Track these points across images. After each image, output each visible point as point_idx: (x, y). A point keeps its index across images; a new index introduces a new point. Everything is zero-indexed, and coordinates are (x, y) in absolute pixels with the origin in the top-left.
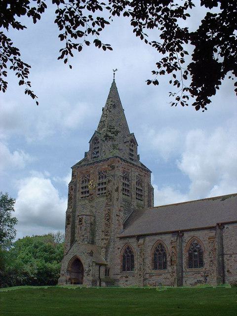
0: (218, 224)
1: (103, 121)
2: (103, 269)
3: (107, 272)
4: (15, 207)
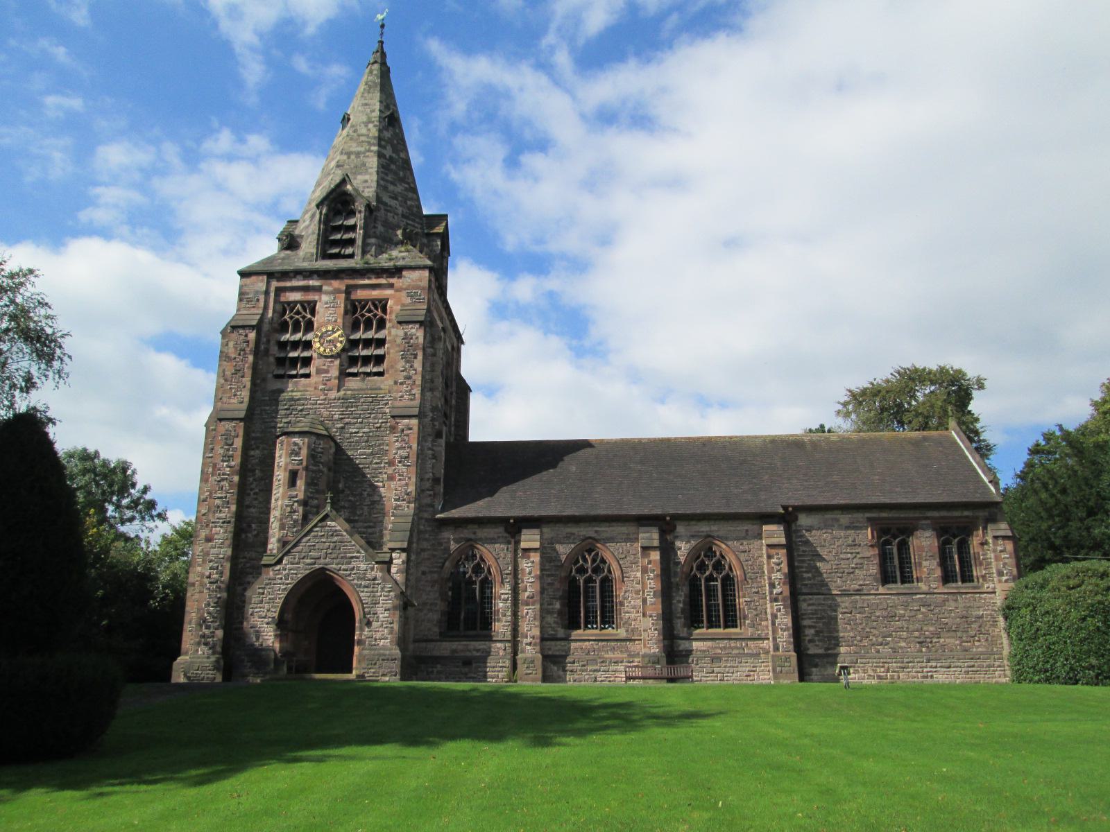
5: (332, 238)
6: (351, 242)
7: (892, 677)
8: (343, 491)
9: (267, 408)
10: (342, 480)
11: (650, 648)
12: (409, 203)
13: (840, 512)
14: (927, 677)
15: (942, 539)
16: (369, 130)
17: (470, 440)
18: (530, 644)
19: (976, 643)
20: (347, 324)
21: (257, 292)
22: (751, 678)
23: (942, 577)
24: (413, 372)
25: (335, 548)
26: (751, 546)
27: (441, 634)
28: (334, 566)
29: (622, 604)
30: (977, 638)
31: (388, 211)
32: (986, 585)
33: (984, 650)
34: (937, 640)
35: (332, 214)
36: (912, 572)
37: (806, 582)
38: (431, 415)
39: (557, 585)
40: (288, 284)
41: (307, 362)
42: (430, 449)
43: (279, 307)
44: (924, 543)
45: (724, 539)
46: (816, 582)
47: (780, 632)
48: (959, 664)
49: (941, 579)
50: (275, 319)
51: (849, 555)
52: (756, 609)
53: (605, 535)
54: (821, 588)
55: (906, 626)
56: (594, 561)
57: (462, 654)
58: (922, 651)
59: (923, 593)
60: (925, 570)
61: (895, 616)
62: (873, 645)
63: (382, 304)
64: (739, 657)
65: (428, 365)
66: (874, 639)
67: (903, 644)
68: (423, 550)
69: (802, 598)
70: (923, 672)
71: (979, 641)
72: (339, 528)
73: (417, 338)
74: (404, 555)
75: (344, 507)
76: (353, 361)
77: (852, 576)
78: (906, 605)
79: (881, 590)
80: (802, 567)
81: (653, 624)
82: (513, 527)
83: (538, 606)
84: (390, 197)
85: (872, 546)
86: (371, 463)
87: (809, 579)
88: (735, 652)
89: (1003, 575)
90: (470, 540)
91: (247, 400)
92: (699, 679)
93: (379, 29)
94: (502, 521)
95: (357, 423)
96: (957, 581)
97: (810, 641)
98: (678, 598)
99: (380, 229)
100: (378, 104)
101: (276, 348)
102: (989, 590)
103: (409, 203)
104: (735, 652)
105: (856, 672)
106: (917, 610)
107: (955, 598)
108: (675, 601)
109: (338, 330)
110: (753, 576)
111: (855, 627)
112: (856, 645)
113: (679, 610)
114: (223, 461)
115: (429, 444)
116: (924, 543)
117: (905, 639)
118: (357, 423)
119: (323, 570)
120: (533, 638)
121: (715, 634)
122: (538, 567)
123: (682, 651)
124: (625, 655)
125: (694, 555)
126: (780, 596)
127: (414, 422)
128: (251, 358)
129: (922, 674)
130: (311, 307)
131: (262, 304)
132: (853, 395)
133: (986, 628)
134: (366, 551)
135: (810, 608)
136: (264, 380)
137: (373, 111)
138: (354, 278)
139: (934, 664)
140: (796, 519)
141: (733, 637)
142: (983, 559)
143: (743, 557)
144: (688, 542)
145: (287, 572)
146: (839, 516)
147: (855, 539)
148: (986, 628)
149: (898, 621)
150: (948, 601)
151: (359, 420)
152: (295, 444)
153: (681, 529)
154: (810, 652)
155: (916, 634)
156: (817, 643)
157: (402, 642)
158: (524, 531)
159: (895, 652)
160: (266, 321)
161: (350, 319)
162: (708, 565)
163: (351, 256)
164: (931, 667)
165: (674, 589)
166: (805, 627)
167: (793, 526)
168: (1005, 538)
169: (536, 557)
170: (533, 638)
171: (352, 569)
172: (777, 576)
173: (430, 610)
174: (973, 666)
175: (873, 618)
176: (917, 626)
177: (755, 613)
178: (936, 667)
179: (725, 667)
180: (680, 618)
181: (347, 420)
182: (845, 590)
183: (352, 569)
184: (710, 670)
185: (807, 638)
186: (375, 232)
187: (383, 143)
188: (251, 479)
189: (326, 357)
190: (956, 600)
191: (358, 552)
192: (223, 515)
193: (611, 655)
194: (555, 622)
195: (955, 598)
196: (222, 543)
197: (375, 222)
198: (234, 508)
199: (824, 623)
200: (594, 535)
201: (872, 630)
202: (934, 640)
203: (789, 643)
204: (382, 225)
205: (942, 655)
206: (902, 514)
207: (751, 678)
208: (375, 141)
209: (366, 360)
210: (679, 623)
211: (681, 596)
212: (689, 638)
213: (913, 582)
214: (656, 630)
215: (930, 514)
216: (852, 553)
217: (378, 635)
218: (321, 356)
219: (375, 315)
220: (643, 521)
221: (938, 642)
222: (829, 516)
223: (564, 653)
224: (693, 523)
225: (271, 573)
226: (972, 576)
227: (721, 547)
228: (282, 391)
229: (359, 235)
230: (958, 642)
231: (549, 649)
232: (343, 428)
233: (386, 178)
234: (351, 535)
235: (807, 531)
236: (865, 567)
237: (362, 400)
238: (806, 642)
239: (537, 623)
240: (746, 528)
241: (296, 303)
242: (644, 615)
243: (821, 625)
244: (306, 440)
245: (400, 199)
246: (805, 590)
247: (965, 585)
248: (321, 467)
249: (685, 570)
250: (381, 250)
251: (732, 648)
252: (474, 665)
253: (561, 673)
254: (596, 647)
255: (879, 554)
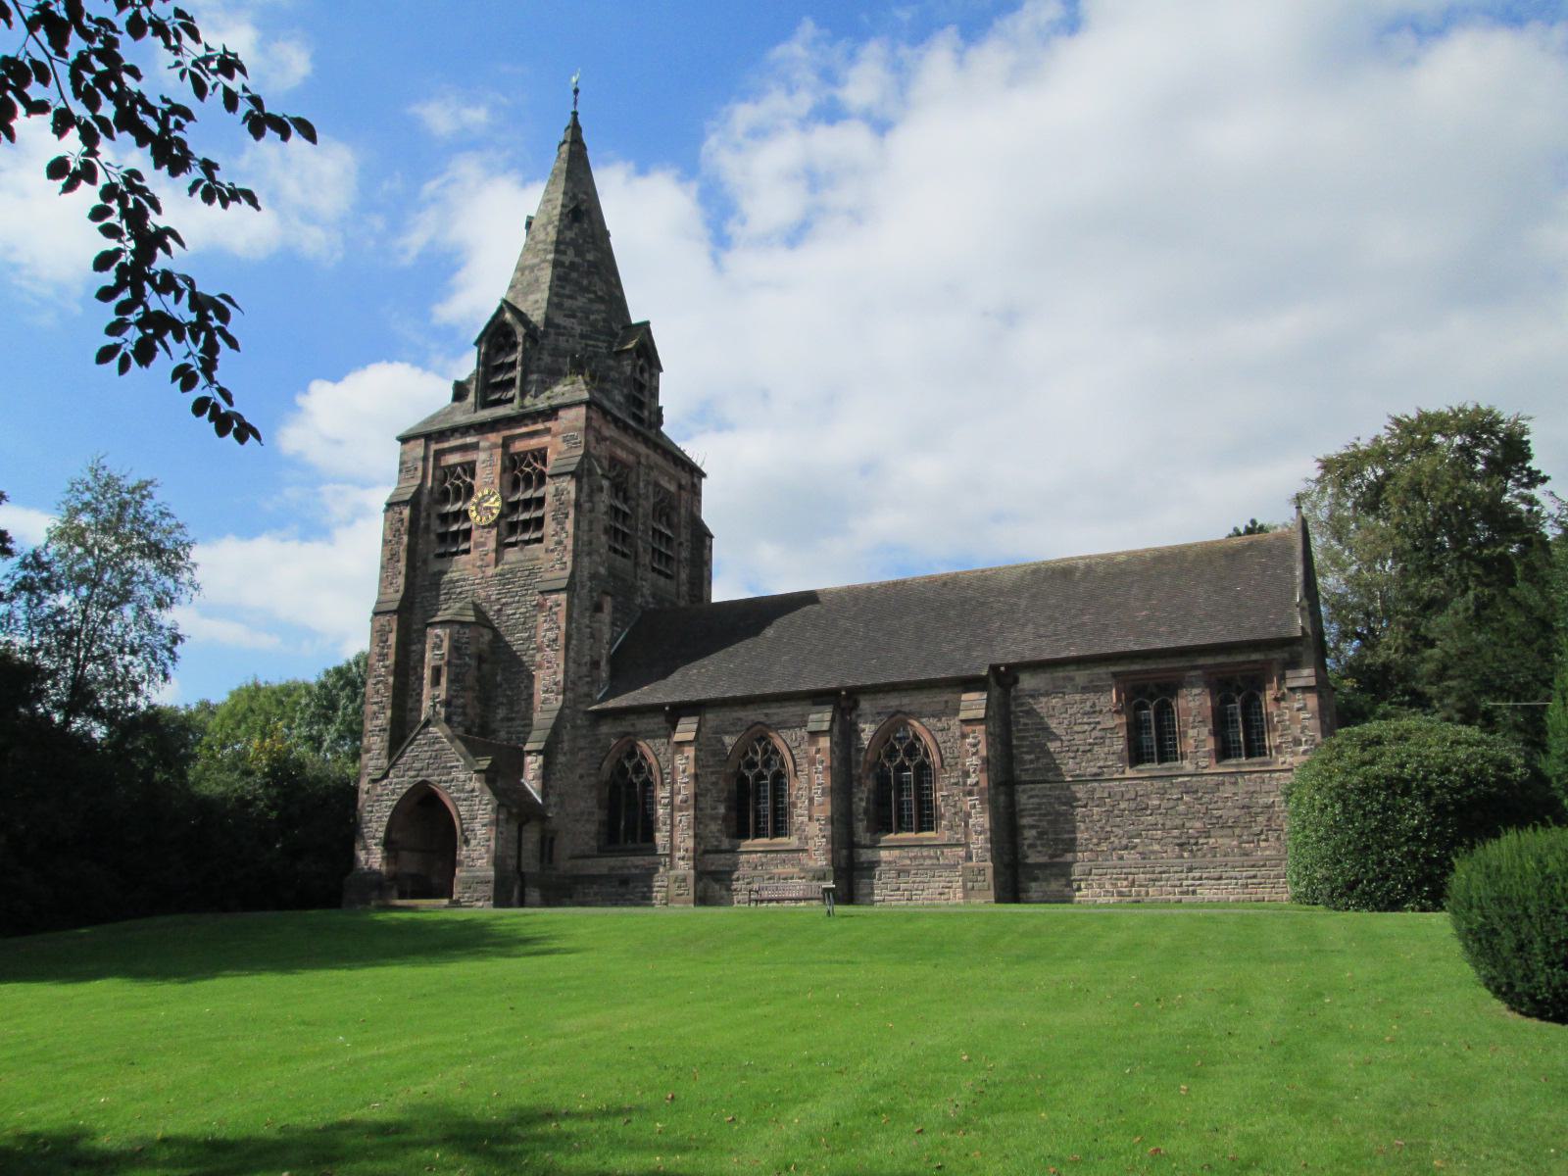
0: (994, 668)
1: (532, 268)
2: (532, 835)
3: (547, 844)
4: (50, 526)
5: (493, 381)
6: (511, 383)
7: (1138, 894)
8: (501, 685)
9: (428, 594)
10: (499, 671)
11: (816, 860)
12: (592, 317)
13: (1074, 668)
14: (1187, 893)
15: (1134, 702)
16: (547, 234)
17: (714, 600)
18: (683, 858)
19: (1263, 844)
20: (505, 484)
21: (416, 459)
22: (946, 897)
23: (1216, 750)
24: (564, 535)
25: (436, 757)
26: (952, 723)
27: (599, 848)
28: (435, 778)
29: (794, 805)
30: (1263, 837)
31: (558, 334)
32: (1281, 760)
33: (1274, 853)
34: (1205, 841)
35: (492, 352)
36: (1176, 746)
37: (1027, 767)
38: (589, 584)
39: (722, 784)
40: (446, 445)
41: (467, 534)
42: (588, 627)
43: (439, 473)
44: (1191, 704)
45: (918, 716)
46: (1040, 765)
47: (975, 837)
48: (1233, 874)
49: (1213, 755)
50: (436, 488)
51: (1086, 727)
52: (955, 806)
53: (776, 719)
54: (1050, 771)
55: (1161, 822)
56: (765, 751)
57: (620, 872)
58: (1182, 857)
59: (1188, 775)
60: (1192, 741)
61: (1146, 809)
62: (1114, 849)
63: (541, 455)
64: (931, 870)
65: (584, 526)
66: (1117, 841)
67: (1156, 847)
68: (581, 749)
69: (1021, 788)
70: (1181, 885)
71: (1266, 840)
72: (440, 734)
73: (569, 493)
74: (540, 758)
75: (502, 704)
76: (513, 528)
77: (1089, 755)
78: (1163, 793)
79: (1129, 773)
80: (1022, 746)
81: (820, 830)
82: (675, 712)
83: (692, 812)
84: (566, 316)
85: (1116, 712)
86: (528, 649)
87: (1031, 762)
88: (928, 862)
89: (1300, 745)
90: (628, 734)
91: (402, 588)
92: (881, 898)
93: (572, 96)
94: (655, 709)
95: (514, 602)
96: (1240, 756)
97: (1031, 846)
98: (860, 795)
99: (547, 359)
100: (561, 197)
101: (438, 522)
102: (1285, 766)
103: (592, 317)
104: (928, 862)
105: (1089, 886)
106: (1178, 799)
107: (1233, 780)
108: (856, 800)
109: (494, 493)
110: (953, 762)
111: (1090, 825)
112: (1092, 850)
113: (861, 811)
114: (379, 661)
115: (587, 621)
116: (1193, 705)
117: (1159, 841)
118: (514, 602)
119: (424, 783)
120: (687, 850)
121: (904, 840)
122: (692, 763)
123: (863, 863)
124: (796, 870)
125: (883, 738)
126: (975, 788)
127: (563, 597)
128: (405, 539)
129: (1180, 889)
130: (470, 468)
131: (420, 473)
132: (1327, 465)
133: (1278, 822)
134: (464, 758)
135: (1032, 800)
136: (425, 562)
137: (555, 208)
138: (510, 428)
139: (1198, 875)
140: (1016, 681)
141: (925, 843)
142: (1278, 722)
143: (939, 737)
144: (872, 722)
145: (392, 787)
146: (1072, 674)
147: (1094, 704)
148: (1278, 822)
149: (1151, 815)
150: (1223, 784)
151: (517, 598)
152: (438, 636)
153: (865, 705)
154: (1030, 861)
155: (1176, 832)
156: (1040, 848)
157: (498, 862)
158: (683, 720)
159: (1144, 859)
160: (426, 491)
161: (508, 477)
162: (898, 751)
163: (511, 400)
164: (1193, 879)
165: (855, 784)
166: (1024, 827)
167: (1013, 693)
168: (1305, 689)
169: (690, 752)
170: (687, 850)
171: (452, 780)
172: (972, 762)
173: (588, 821)
174: (1255, 877)
175: (1116, 812)
176: (1178, 822)
177: (953, 811)
178: (1201, 879)
179: (914, 882)
180: (861, 820)
181: (504, 600)
182: (1078, 776)
183: (452, 780)
184: (895, 887)
185: (1026, 842)
186: (538, 367)
187: (562, 247)
188: (413, 678)
189: (484, 527)
190: (1235, 783)
191: (458, 760)
192: (379, 722)
193: (780, 870)
194: (719, 831)
195: (1233, 780)
196: (379, 754)
197: (540, 353)
198: (389, 713)
199: (1049, 822)
200: (762, 719)
201: (1114, 829)
202: (1201, 841)
203: (986, 850)
204: (550, 355)
205: (1212, 862)
206: (1163, 665)
207: (946, 897)
208: (552, 248)
209: (526, 525)
210: (860, 826)
211: (863, 792)
212: (874, 846)
213: (1176, 760)
214: (824, 837)
215: (1201, 661)
216: (1089, 724)
217: (475, 855)
218: (478, 527)
219: (535, 469)
220: (818, 697)
221: (1207, 843)
222: (1060, 674)
223: (728, 869)
224: (881, 695)
225: (379, 788)
226: (1265, 747)
227: (644, 746)
228: (446, 573)
229: (517, 373)
230: (1235, 843)
231: (712, 864)
232: (500, 610)
233: (562, 291)
234: (451, 741)
235: (1032, 696)
236: (1107, 741)
237: (519, 574)
238: (1025, 848)
239: (691, 833)
240: (945, 698)
241: (455, 466)
242: (810, 819)
243: (1045, 824)
244: (448, 631)
245: (579, 315)
246: (1025, 777)
247: (1251, 760)
248: (467, 659)
249: (868, 758)
250: (544, 386)
251: (924, 858)
252: (632, 885)
253: (724, 892)
254: (764, 860)
255: (1128, 724)
